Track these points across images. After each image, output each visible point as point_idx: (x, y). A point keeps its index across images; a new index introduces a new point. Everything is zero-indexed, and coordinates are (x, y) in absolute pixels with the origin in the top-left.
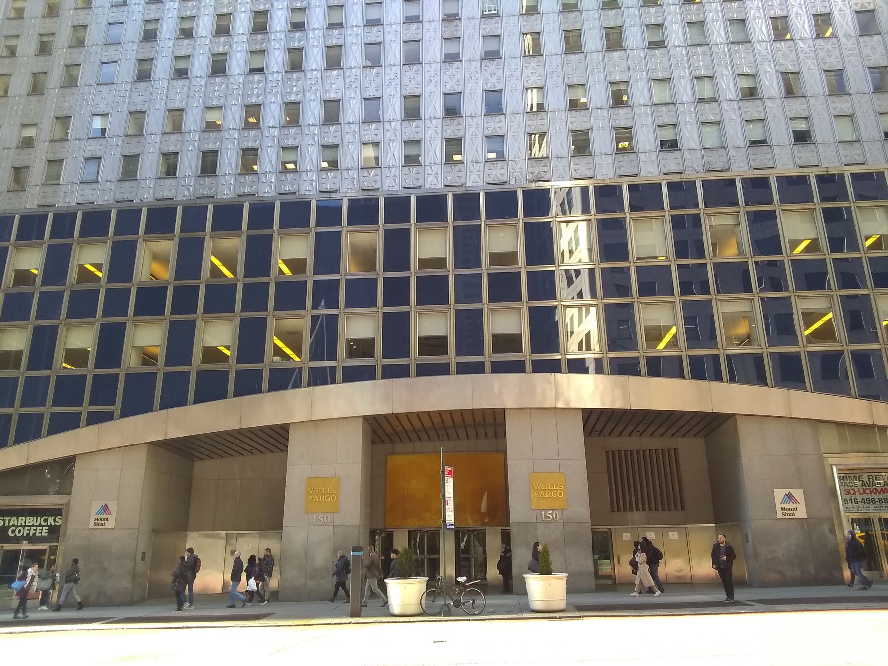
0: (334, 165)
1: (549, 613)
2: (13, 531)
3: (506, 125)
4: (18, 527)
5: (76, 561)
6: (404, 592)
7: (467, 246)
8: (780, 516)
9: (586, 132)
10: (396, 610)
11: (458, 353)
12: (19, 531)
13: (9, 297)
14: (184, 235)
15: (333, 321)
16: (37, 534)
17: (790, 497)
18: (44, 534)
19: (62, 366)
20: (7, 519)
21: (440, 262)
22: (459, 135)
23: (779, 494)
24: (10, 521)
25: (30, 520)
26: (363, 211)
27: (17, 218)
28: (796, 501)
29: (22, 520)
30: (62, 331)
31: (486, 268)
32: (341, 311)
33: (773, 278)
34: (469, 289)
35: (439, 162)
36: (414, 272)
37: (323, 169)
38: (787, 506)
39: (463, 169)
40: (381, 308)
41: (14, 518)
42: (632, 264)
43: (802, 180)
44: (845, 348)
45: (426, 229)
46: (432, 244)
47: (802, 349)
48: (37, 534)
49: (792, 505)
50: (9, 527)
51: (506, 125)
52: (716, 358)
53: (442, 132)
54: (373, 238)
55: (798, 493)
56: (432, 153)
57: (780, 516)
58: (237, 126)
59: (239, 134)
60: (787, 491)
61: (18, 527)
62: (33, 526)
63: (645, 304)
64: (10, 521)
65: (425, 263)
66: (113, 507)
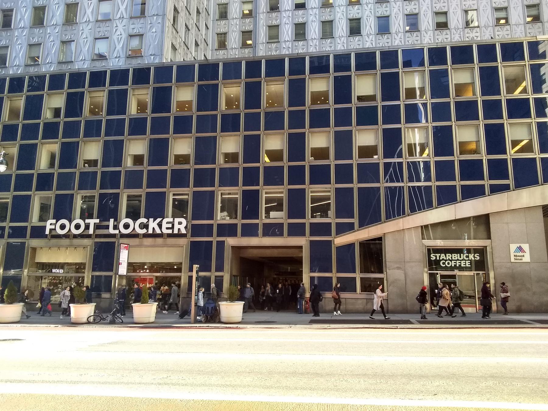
0: (537, 19)
1: (146, 325)
2: (444, 263)
3: (419, 7)
4: (446, 260)
5: (503, 284)
6: (82, 311)
7: (297, 91)
8: (513, 260)
9: (331, 22)
10: (223, 320)
11: (336, 158)
12: (448, 264)
13: (5, 127)
14: (201, 83)
15: (166, 142)
16: (462, 266)
17: (520, 249)
18: (467, 266)
19: (309, 160)
20: (438, 255)
21: (372, 98)
22: (387, 14)
23: (513, 247)
24: (440, 256)
25: (455, 256)
26: (97, 79)
27: (263, 62)
28: (524, 252)
29: (449, 256)
30: (219, 141)
31: (354, 104)
32: (354, 128)
33: (493, 109)
34: (297, 119)
35: (373, 32)
36: (354, 104)
37: (528, 23)
38: (518, 254)
39: (390, 38)
40: (149, 135)
41: (443, 255)
42: (452, 100)
43: (520, 45)
44: (381, 161)
45: (271, 81)
46: (275, 89)
47: (456, 158)
48: (462, 266)
49: (521, 254)
50: (440, 261)
51: (419, 7)
52: (400, 164)
53: (320, 17)
54: (101, 96)
55: (526, 247)
56: (397, 25)
57: (513, 260)
58: (317, 6)
59: (292, 13)
60: (518, 245)
61: (446, 260)
62: (458, 260)
63: (459, 126)
64: (440, 256)
65: (360, 99)
66: (526, 247)
